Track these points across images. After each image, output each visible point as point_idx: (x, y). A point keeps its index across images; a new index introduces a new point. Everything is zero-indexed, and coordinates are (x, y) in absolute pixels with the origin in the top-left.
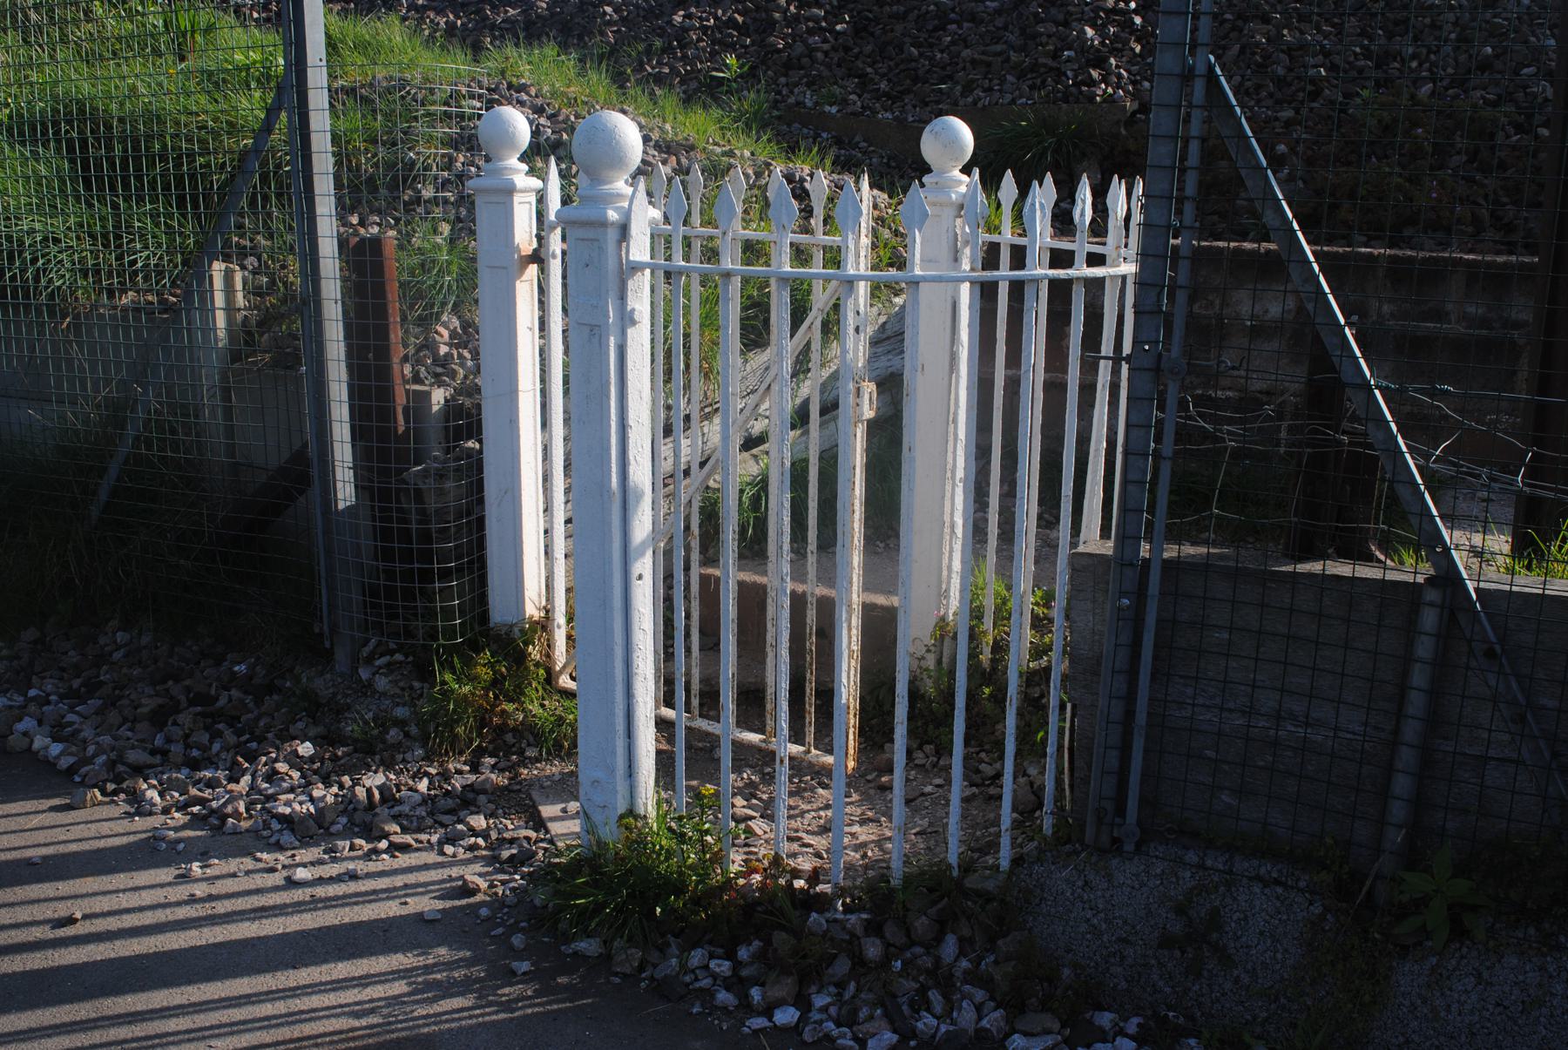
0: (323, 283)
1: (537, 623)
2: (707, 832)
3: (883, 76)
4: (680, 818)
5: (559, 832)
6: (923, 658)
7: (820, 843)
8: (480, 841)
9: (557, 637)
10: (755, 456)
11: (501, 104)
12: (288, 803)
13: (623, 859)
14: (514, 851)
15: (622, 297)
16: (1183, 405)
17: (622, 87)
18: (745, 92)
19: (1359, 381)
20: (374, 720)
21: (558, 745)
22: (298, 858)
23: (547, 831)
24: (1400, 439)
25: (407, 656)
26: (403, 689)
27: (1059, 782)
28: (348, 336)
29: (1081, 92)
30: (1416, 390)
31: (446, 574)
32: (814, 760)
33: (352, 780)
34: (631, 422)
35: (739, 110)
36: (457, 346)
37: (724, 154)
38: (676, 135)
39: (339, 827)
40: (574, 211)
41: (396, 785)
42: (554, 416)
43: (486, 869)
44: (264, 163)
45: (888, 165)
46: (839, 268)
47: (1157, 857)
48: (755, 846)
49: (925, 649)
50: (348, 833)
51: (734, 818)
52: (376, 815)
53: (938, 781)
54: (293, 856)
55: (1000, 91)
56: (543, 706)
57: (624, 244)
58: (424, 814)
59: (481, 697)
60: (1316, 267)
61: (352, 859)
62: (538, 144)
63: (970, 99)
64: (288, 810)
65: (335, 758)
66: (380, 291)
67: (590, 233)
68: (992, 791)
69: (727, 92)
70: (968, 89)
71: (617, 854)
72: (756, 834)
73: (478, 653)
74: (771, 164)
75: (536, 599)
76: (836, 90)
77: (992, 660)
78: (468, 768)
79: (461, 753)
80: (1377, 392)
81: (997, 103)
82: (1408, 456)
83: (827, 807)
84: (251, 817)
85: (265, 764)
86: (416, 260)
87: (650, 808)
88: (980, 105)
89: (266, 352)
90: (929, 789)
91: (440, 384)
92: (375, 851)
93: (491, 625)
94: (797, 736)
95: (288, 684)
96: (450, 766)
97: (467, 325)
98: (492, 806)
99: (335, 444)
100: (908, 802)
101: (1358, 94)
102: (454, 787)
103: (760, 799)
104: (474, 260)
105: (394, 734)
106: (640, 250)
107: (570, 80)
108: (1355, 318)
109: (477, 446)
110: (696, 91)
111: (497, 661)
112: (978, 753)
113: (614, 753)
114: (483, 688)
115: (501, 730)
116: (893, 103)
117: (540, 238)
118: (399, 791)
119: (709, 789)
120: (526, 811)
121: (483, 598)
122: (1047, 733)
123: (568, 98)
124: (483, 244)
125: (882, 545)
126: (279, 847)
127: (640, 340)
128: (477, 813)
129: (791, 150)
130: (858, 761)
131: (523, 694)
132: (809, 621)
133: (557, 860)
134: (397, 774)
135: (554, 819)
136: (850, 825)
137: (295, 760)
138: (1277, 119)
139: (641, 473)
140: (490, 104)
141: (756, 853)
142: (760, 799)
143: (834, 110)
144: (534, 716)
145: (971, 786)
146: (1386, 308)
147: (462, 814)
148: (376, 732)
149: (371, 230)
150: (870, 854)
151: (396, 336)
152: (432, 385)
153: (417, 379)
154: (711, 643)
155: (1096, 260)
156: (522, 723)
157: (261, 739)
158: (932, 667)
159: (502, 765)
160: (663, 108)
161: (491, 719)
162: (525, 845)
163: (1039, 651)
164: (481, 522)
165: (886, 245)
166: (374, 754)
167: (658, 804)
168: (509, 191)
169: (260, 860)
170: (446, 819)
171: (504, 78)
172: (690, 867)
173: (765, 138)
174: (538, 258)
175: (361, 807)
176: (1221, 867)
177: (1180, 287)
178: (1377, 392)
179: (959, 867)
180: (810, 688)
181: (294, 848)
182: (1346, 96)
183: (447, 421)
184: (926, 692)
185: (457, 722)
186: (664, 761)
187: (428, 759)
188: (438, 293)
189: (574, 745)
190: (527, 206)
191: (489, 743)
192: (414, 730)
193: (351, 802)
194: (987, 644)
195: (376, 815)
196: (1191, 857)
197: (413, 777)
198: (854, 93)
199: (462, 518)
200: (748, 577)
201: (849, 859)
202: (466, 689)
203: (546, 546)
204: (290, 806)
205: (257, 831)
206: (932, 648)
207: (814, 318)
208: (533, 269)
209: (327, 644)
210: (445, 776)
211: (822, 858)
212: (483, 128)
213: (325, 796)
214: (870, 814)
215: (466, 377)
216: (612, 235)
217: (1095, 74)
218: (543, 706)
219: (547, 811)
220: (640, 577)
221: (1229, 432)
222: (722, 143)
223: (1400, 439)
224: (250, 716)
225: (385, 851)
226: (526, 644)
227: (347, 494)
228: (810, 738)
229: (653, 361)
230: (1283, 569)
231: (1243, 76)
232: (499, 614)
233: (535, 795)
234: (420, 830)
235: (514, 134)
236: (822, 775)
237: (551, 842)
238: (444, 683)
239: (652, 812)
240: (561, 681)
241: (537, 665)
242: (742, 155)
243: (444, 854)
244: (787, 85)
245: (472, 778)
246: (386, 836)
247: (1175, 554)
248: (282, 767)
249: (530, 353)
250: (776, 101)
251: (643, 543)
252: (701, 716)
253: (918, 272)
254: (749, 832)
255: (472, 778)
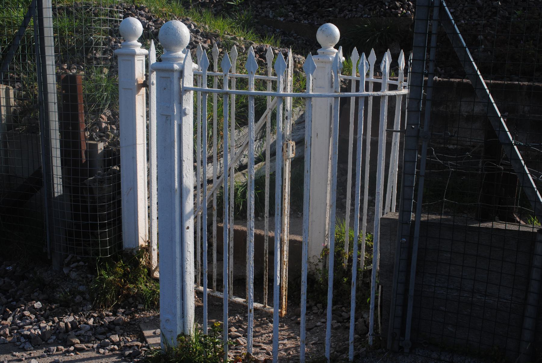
0: (49, 95)
1: (144, 248)
2: (217, 343)
3: (304, 4)
4: (205, 337)
5: (152, 343)
6: (317, 265)
7: (269, 348)
8: (116, 347)
9: (153, 255)
10: (244, 174)
11: (132, 16)
12: (29, 330)
13: (179, 355)
14: (131, 352)
15: (180, 103)
16: (429, 152)
17: (187, 8)
18: (243, 11)
19: (507, 142)
20: (70, 291)
21: (153, 303)
22: (32, 355)
23: (146, 342)
24: (526, 168)
25: (85, 263)
26: (83, 278)
27: (376, 321)
28: (60, 119)
29: (392, 12)
30: (534, 146)
31: (103, 226)
32: (267, 310)
33: (58, 319)
34: (184, 159)
35: (240, 19)
36: (110, 124)
37: (232, 39)
38: (211, 30)
39: (52, 340)
40: (163, 65)
41: (79, 321)
42: (152, 142)
43: (118, 360)
44: (23, 41)
45: (306, 44)
46: (276, 91)
47: (419, 355)
48: (240, 349)
49: (318, 261)
50: (56, 344)
51: (230, 336)
52: (69, 335)
53: (323, 320)
54: (30, 354)
55: (355, 11)
56: (146, 285)
57: (181, 80)
58: (91, 334)
59: (118, 281)
60: (488, 91)
61: (57, 355)
62: (148, 34)
63: (342, 15)
64: (29, 333)
65: (51, 309)
66: (75, 99)
67: (165, 75)
68: (347, 325)
69: (234, 11)
70: (342, 10)
71: (176, 353)
72: (240, 344)
73: (117, 262)
74: (252, 44)
75: (144, 237)
76: (283, 10)
77: (348, 266)
78: (111, 314)
79: (109, 307)
80: (515, 147)
81: (354, 17)
82: (529, 175)
83: (272, 332)
84: (12, 336)
85: (19, 312)
86: (93, 85)
87: (192, 332)
88: (347, 17)
89: (24, 125)
90: (319, 324)
91: (102, 140)
92: (68, 352)
93: (124, 249)
94: (258, 298)
95: (31, 275)
96: (104, 313)
97: (115, 114)
98: (122, 331)
99: (54, 167)
100: (308, 330)
101: (515, 13)
102: (105, 322)
103: (243, 328)
104: (117, 85)
105: (78, 298)
106: (188, 82)
107: (164, 5)
108: (506, 114)
109: (118, 168)
110: (220, 10)
111: (126, 265)
112: (341, 308)
113: (176, 307)
114: (119, 278)
115: (127, 296)
116: (308, 16)
117: (146, 76)
118: (80, 324)
119: (218, 324)
120: (137, 333)
121: (120, 237)
122: (370, 298)
123: (163, 13)
124: (121, 78)
125: (300, 214)
126: (24, 350)
127: (188, 122)
128: (115, 334)
129: (262, 37)
130: (287, 311)
131: (137, 280)
132: (265, 248)
133: (150, 356)
134: (79, 316)
135: (150, 337)
136: (283, 340)
137: (33, 310)
138: (479, 24)
139: (189, 180)
140: (126, 16)
141: (240, 353)
142: (243, 328)
143: (282, 19)
144: (142, 290)
145: (338, 322)
146: (526, 109)
147: (108, 335)
148: (70, 297)
149: (73, 71)
150: (291, 353)
151: (82, 119)
152: (98, 141)
153: (91, 138)
154: (220, 259)
155: (393, 87)
156: (136, 293)
157: (18, 301)
158: (321, 269)
159: (127, 312)
160: (205, 18)
161: (123, 292)
162: (136, 348)
163: (369, 262)
164: (119, 202)
165: (303, 80)
166: (69, 307)
167: (196, 330)
168: (133, 55)
169: (15, 356)
170: (100, 337)
171: (134, 4)
172: (209, 359)
173: (250, 32)
174: (146, 84)
175: (62, 331)
176: (448, 360)
177: (428, 100)
178: (515, 147)
179: (330, 359)
180: (266, 278)
181: (31, 350)
182: (510, 14)
183: (105, 157)
184: (319, 280)
185: (107, 293)
186: (198, 310)
187: (94, 309)
188: (102, 100)
189: (158, 304)
190: (141, 62)
191: (122, 302)
192: (87, 296)
193: (58, 329)
194: (346, 258)
195: (69, 335)
196: (435, 355)
197: (87, 318)
198: (291, 12)
199: (111, 201)
200: (239, 227)
201: (281, 355)
202: (111, 278)
203: (149, 214)
204: (30, 331)
205: (14, 343)
206: (321, 260)
207: (268, 113)
208: (143, 90)
209: (49, 258)
210: (101, 317)
211: (269, 355)
212: (122, 26)
213: (46, 326)
214: (292, 335)
215: (114, 138)
216: (176, 75)
217: (398, 4)
218: (146, 285)
219: (147, 333)
220: (188, 228)
221: (451, 165)
222: (231, 34)
223: (526, 168)
224: (13, 290)
225: (73, 352)
226: (139, 257)
227: (59, 190)
228: (266, 300)
229: (195, 132)
230: (475, 225)
231: (464, 5)
232: (127, 244)
233: (142, 326)
234: (89, 342)
235: (135, 29)
236: (270, 316)
237: (148, 347)
238: (101, 275)
239: (193, 334)
240: (155, 274)
241: (144, 267)
242: (240, 39)
243: (99, 353)
244: (261, 8)
245: (113, 318)
246: (73, 344)
247: (426, 219)
248: (27, 313)
249: (142, 127)
250: (256, 15)
251: (190, 213)
252: (217, 290)
253: (311, 93)
254: (238, 343)
255: (113, 318)
